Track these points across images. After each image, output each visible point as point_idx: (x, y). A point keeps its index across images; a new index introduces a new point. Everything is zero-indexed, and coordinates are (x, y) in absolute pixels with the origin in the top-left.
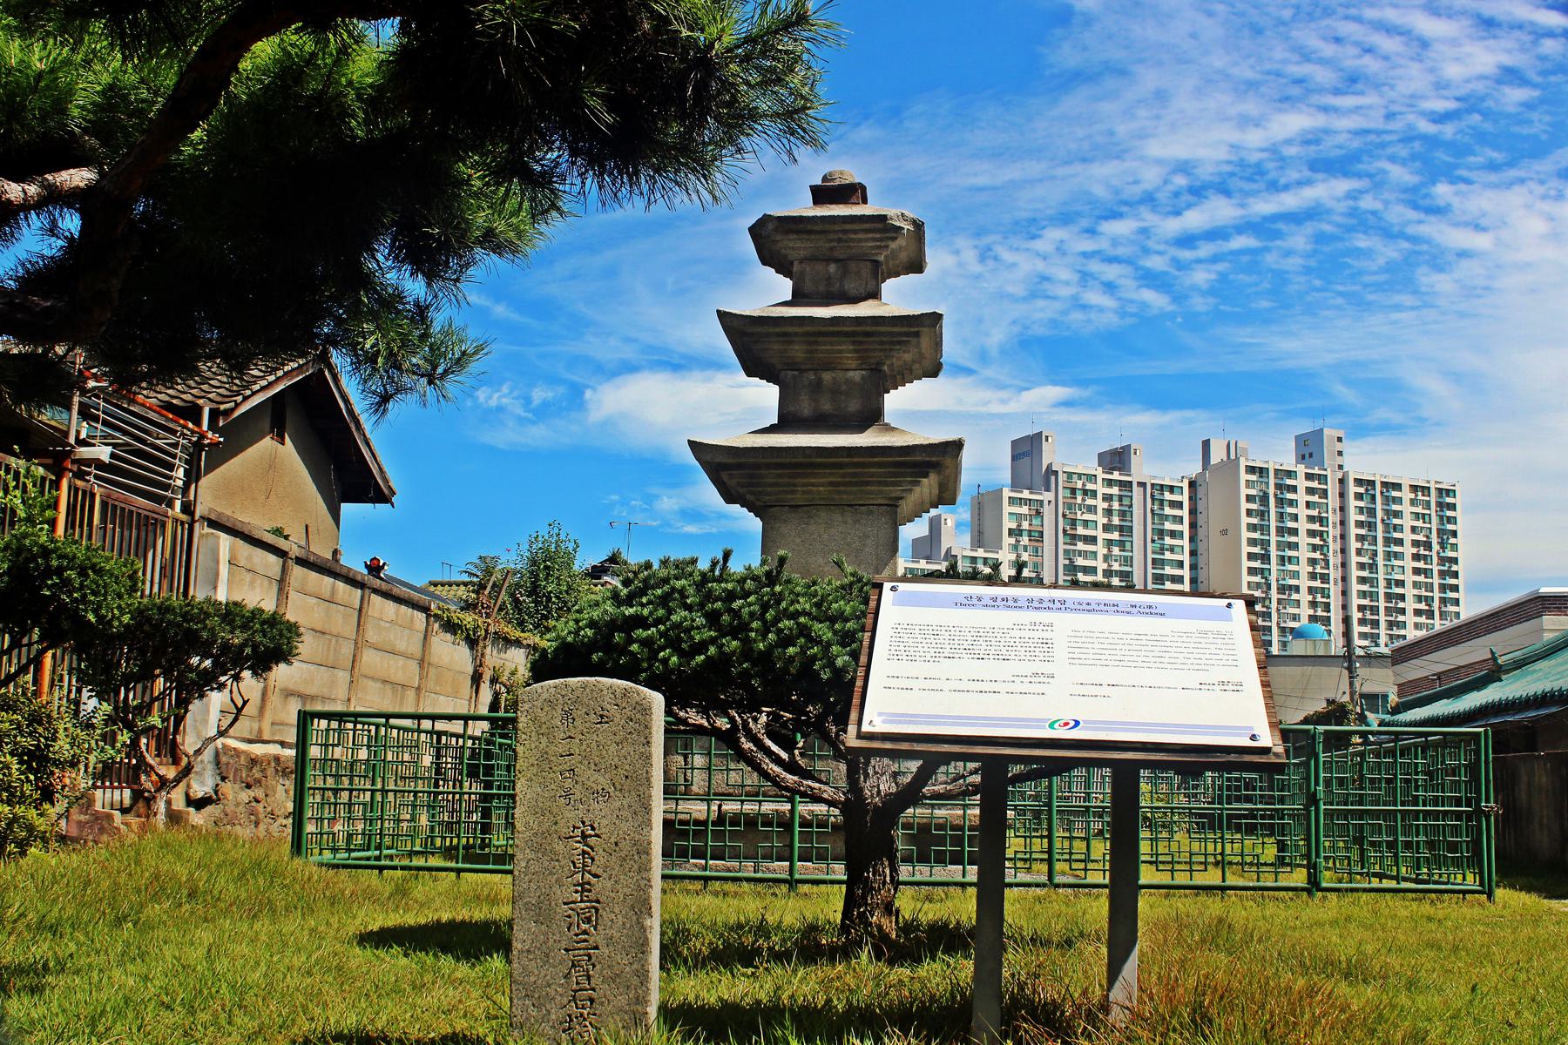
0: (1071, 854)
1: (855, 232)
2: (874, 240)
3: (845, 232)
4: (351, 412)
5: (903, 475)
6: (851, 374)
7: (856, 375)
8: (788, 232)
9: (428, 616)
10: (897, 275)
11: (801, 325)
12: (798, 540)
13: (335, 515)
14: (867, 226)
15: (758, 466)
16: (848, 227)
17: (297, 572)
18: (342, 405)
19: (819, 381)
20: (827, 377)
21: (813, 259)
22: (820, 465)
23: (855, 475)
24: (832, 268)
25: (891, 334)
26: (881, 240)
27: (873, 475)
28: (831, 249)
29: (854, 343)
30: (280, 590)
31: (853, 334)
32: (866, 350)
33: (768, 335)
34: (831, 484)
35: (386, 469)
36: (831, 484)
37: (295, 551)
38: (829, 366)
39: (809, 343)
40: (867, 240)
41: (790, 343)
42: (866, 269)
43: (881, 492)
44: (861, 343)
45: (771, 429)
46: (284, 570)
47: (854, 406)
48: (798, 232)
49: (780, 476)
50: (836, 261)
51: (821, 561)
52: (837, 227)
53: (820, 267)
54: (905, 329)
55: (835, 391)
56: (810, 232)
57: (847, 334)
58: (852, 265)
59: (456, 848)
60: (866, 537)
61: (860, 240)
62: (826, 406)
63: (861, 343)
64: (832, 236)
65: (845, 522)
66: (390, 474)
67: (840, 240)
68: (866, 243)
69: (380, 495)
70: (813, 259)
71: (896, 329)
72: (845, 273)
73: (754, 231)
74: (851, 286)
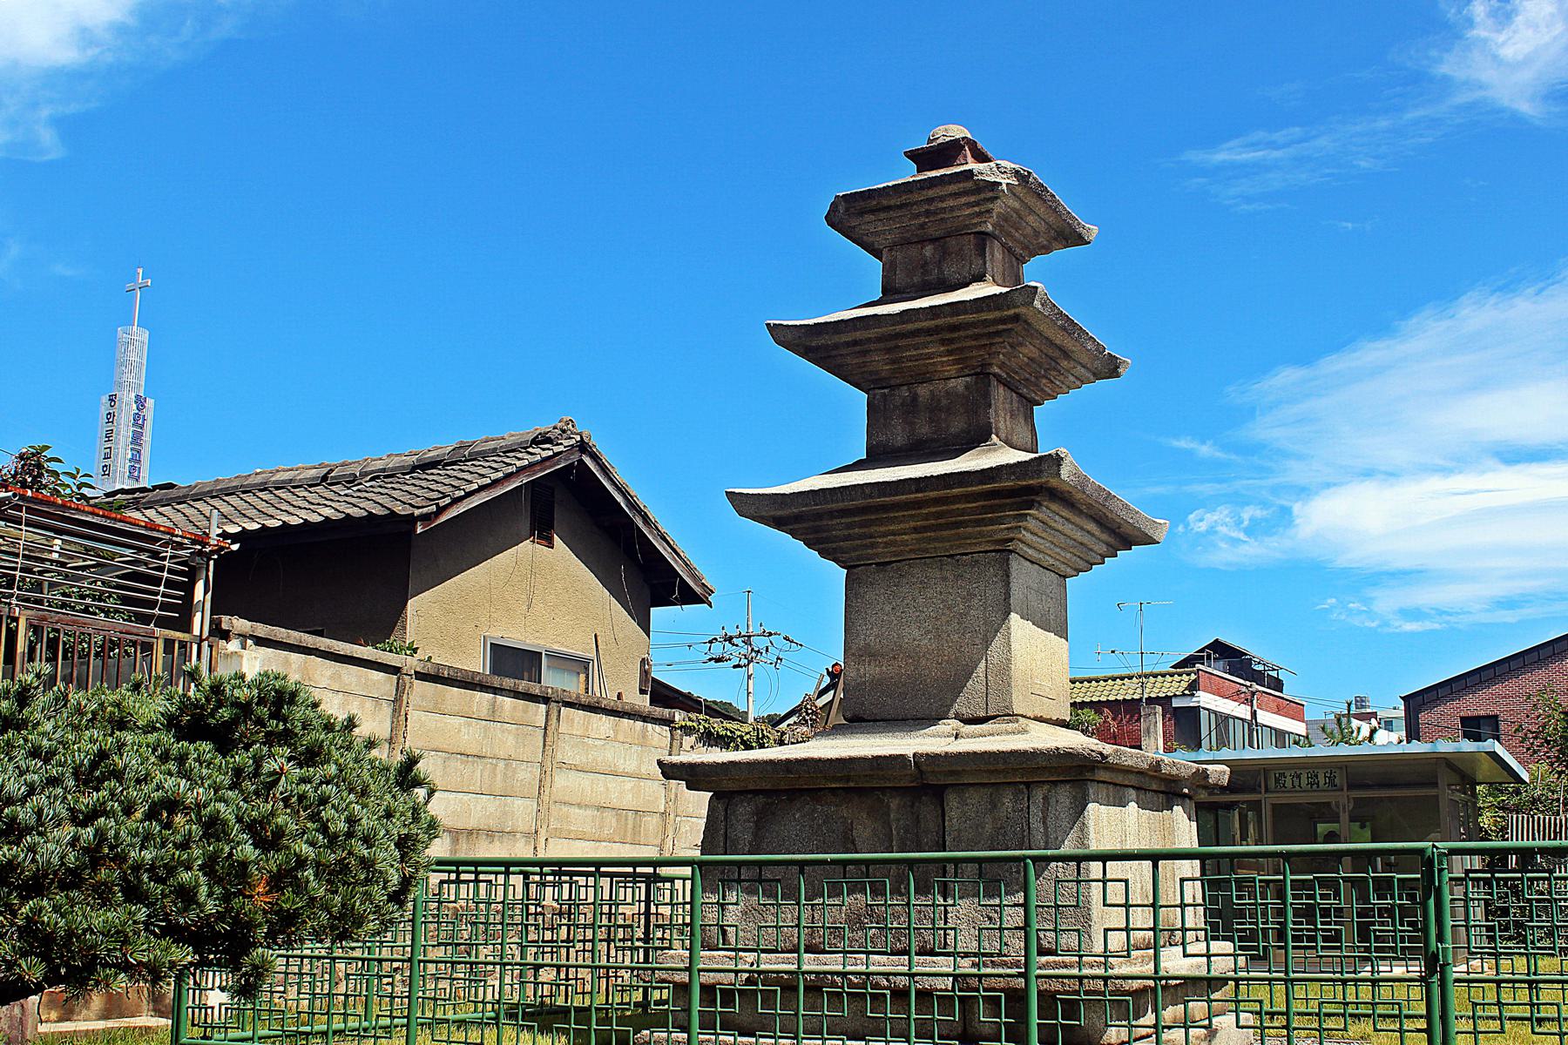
0: (1401, 1031)
1: (942, 199)
2: (969, 205)
3: (930, 200)
4: (633, 506)
5: (1002, 508)
6: (952, 383)
7: (958, 384)
8: (862, 213)
9: (672, 730)
10: (1047, 249)
11: (867, 328)
12: (888, 608)
13: (645, 625)
14: (953, 188)
15: (819, 516)
16: (931, 193)
17: (422, 691)
18: (619, 498)
19: (915, 398)
20: (923, 391)
21: (905, 243)
22: (884, 508)
23: (939, 515)
24: (928, 251)
25: (985, 323)
26: (977, 204)
27: (963, 512)
28: (922, 226)
29: (943, 342)
30: (396, 712)
31: (937, 330)
32: (961, 350)
33: (836, 346)
34: (916, 530)
35: (694, 563)
36: (916, 530)
37: (411, 663)
38: (924, 377)
39: (888, 351)
40: (960, 207)
41: (865, 353)
42: (969, 244)
43: (981, 534)
44: (951, 341)
45: (858, 466)
46: (400, 690)
47: (957, 425)
48: (872, 211)
49: (849, 526)
50: (933, 240)
51: (916, 633)
52: (916, 197)
53: (913, 251)
54: (997, 314)
55: (934, 408)
56: (888, 208)
57: (929, 332)
58: (952, 242)
59: (588, 1009)
60: (971, 595)
61: (952, 209)
62: (924, 430)
63: (951, 341)
64: (916, 210)
65: (944, 579)
66: (701, 570)
67: (928, 213)
68: (961, 209)
69: (690, 596)
70: (905, 243)
71: (984, 316)
72: (945, 254)
73: (832, 220)
74: (951, 271)
